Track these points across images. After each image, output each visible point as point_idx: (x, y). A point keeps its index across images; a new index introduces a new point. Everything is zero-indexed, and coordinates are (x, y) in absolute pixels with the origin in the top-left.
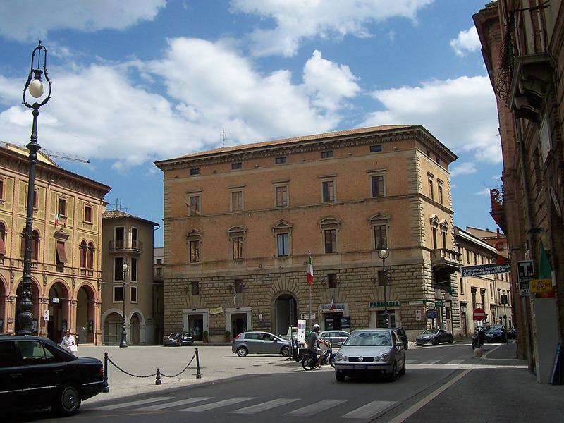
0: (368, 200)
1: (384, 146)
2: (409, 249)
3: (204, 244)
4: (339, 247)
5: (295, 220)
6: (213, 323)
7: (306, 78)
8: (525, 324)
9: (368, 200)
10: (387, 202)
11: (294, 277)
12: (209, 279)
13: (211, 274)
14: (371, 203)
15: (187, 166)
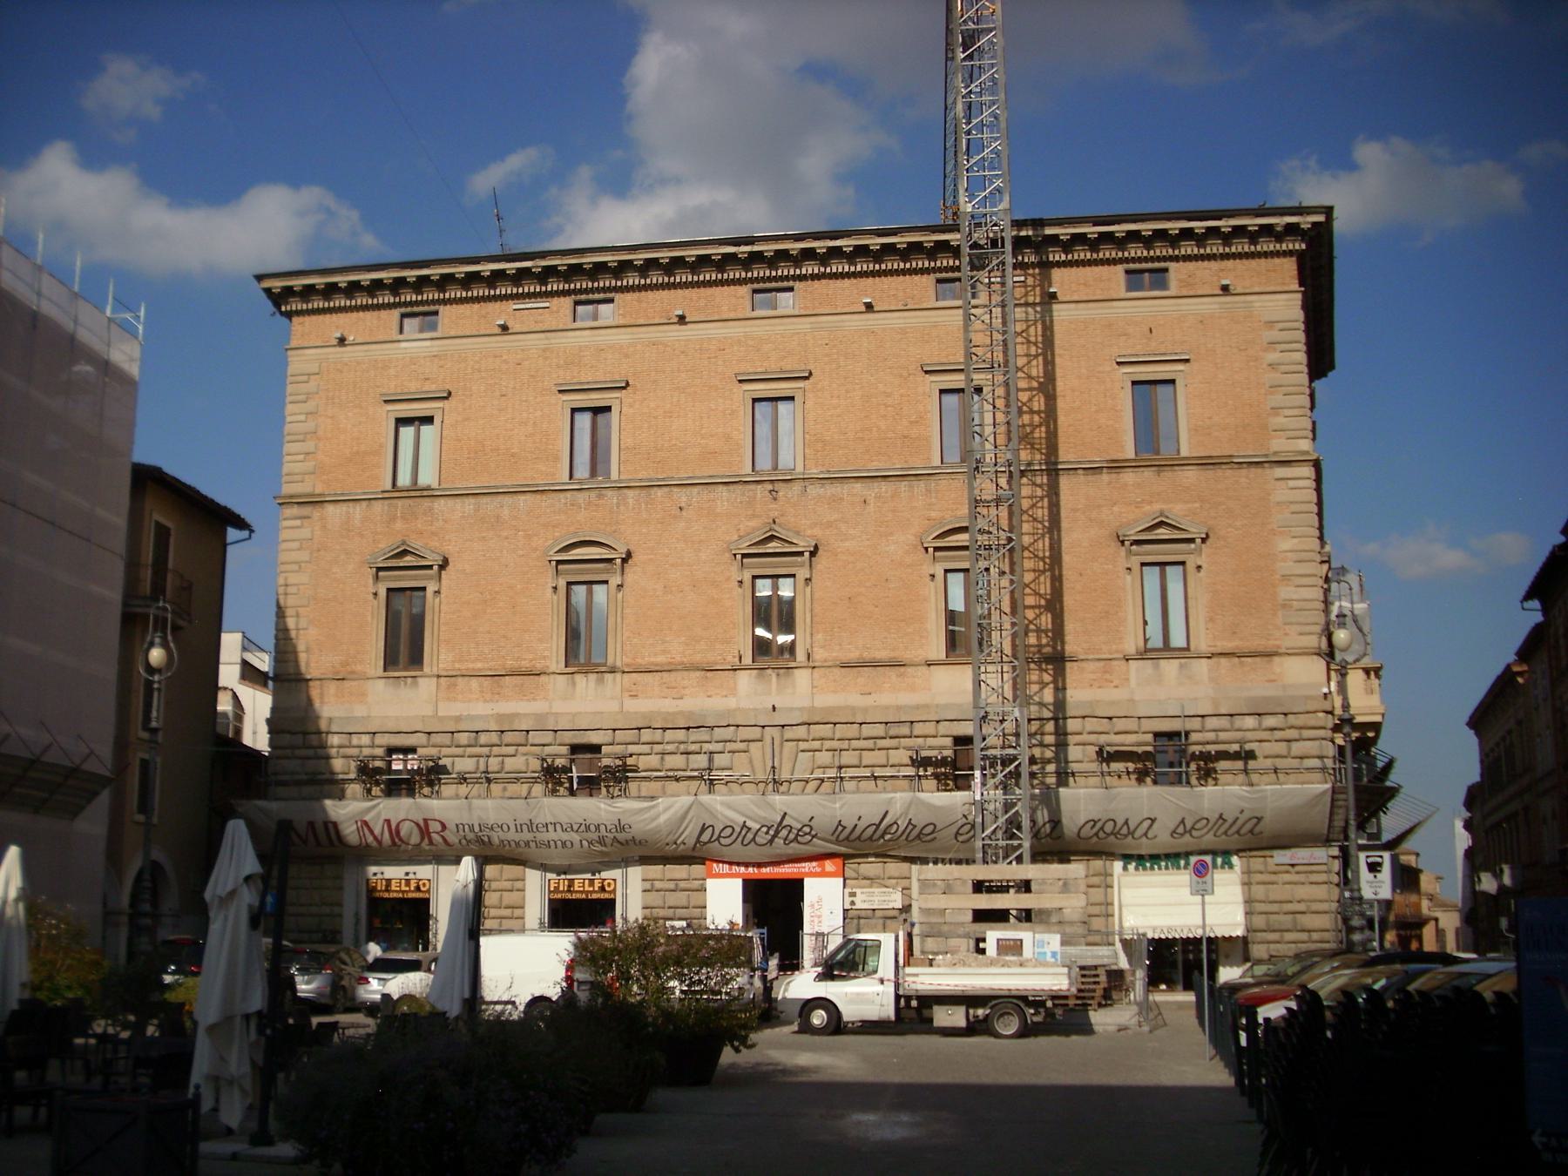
0: (1116, 466)
1: (1177, 272)
2: (1269, 655)
3: (446, 610)
5: (829, 525)
7: (1096, 1028)
9: (1116, 466)
10: (1190, 475)
12: (463, 738)
13: (472, 718)
14: (1129, 477)
15: (389, 298)
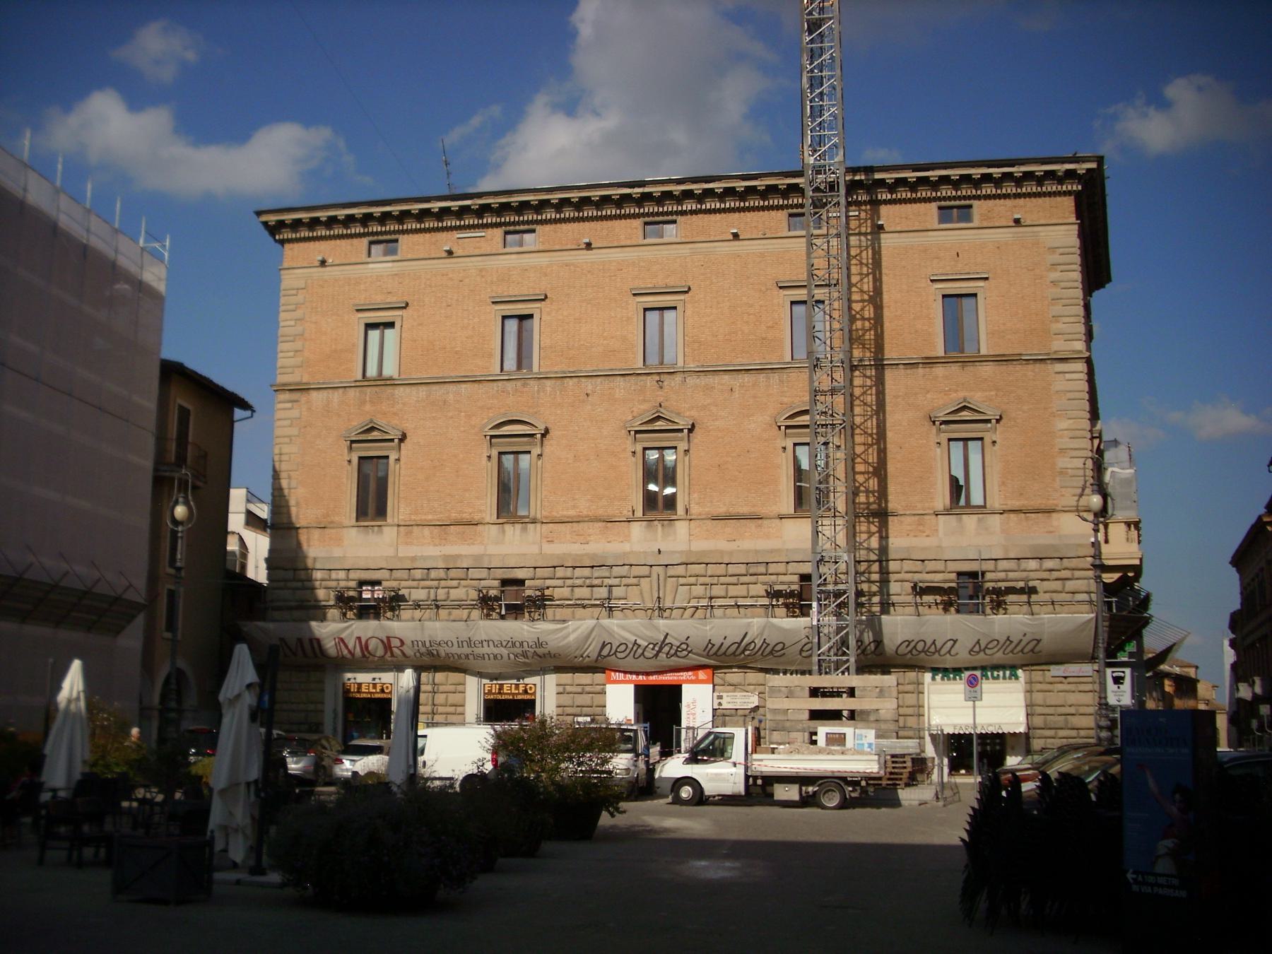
0: (930, 362)
2: (1049, 511)
4: (541, 497)
5: (704, 408)
6: (569, 710)
8: (580, 719)
9: (930, 362)
10: (987, 370)
11: (693, 580)
12: (418, 574)
13: (424, 558)
14: (939, 371)
